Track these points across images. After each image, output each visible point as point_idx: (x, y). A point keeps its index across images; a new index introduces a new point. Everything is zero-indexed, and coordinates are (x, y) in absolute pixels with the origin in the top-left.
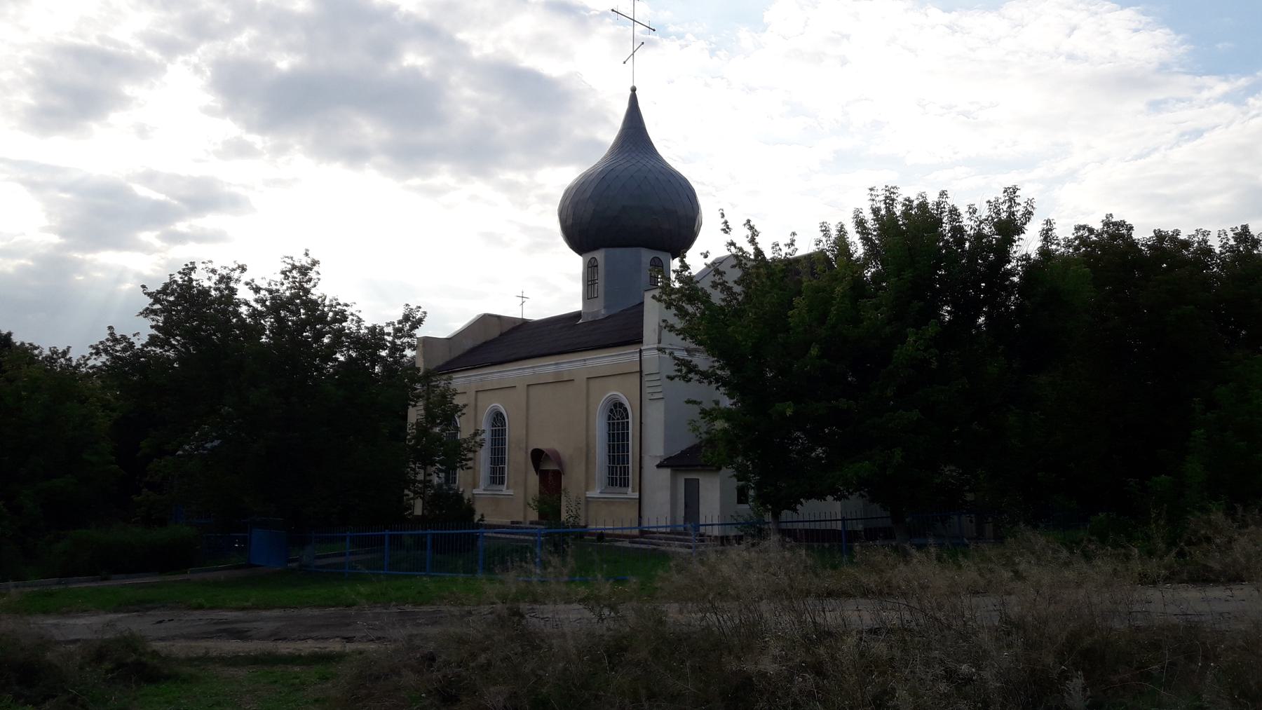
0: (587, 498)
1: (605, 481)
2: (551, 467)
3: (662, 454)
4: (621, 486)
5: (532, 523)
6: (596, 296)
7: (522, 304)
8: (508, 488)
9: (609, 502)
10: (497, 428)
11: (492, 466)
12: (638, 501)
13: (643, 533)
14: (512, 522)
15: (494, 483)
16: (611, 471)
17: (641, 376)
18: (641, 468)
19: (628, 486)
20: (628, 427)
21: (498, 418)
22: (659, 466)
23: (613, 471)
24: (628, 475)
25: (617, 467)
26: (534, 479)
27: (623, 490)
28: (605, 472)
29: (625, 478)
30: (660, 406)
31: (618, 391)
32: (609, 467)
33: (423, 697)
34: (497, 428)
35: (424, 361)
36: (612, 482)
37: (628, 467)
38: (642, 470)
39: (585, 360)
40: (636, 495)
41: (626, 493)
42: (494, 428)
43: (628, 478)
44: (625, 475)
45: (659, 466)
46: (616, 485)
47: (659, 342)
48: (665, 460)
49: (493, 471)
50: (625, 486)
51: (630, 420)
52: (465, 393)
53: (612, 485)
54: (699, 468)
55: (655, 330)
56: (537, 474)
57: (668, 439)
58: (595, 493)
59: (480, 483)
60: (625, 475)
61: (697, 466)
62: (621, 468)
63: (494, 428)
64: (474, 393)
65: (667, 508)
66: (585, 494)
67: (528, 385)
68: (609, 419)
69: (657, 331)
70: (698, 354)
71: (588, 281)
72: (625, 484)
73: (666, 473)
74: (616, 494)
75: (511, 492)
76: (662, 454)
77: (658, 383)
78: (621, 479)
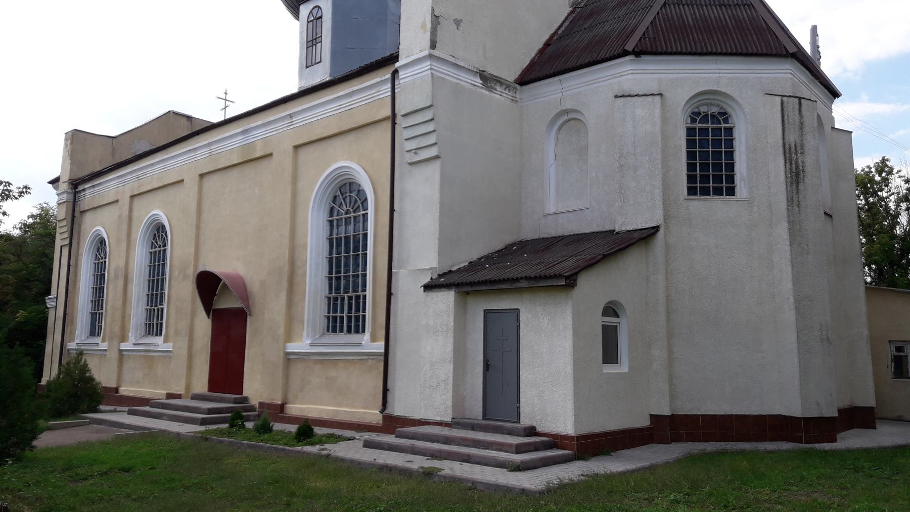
0: (287, 354)
1: (322, 323)
2: (225, 303)
3: (435, 264)
4: (349, 331)
5: (196, 397)
6: (318, 60)
7: (225, 108)
8: (166, 340)
9: (325, 360)
10: (157, 249)
11: (149, 307)
12: (382, 358)
13: (392, 424)
14: (170, 396)
15: (149, 334)
16: (333, 304)
17: (394, 124)
18: (389, 294)
19: (364, 331)
20: (364, 285)
21: (158, 233)
22: (428, 287)
23: (335, 305)
24: (364, 310)
25: (343, 299)
26: (204, 324)
27: (354, 338)
28: (322, 309)
29: (357, 318)
30: (433, 172)
31: (347, 159)
32: (329, 298)
33: (487, 267)
34: (157, 249)
35: (71, 164)
36: (334, 325)
37: (365, 297)
38: (393, 298)
39: (291, 116)
40: (379, 347)
41: (360, 345)
42: (154, 250)
43: (364, 317)
44: (357, 310)
45: (428, 287)
46: (342, 331)
47: (433, 45)
48: (440, 276)
49: (150, 313)
50: (357, 332)
51: (371, 212)
52: (117, 201)
53: (334, 331)
54: (524, 284)
55: (423, 26)
56: (208, 315)
57: (446, 242)
58: (301, 345)
59: (130, 334)
60: (357, 310)
61: (517, 280)
62: (350, 298)
63: (154, 250)
64: (128, 200)
65: (447, 370)
66: (285, 347)
67: (202, 176)
68: (331, 214)
69: (429, 26)
70: (498, 88)
71: (307, 42)
72: (357, 327)
73: (446, 299)
74: (342, 343)
75: (169, 347)
76: (435, 264)
77: (430, 127)
78: (349, 318)
